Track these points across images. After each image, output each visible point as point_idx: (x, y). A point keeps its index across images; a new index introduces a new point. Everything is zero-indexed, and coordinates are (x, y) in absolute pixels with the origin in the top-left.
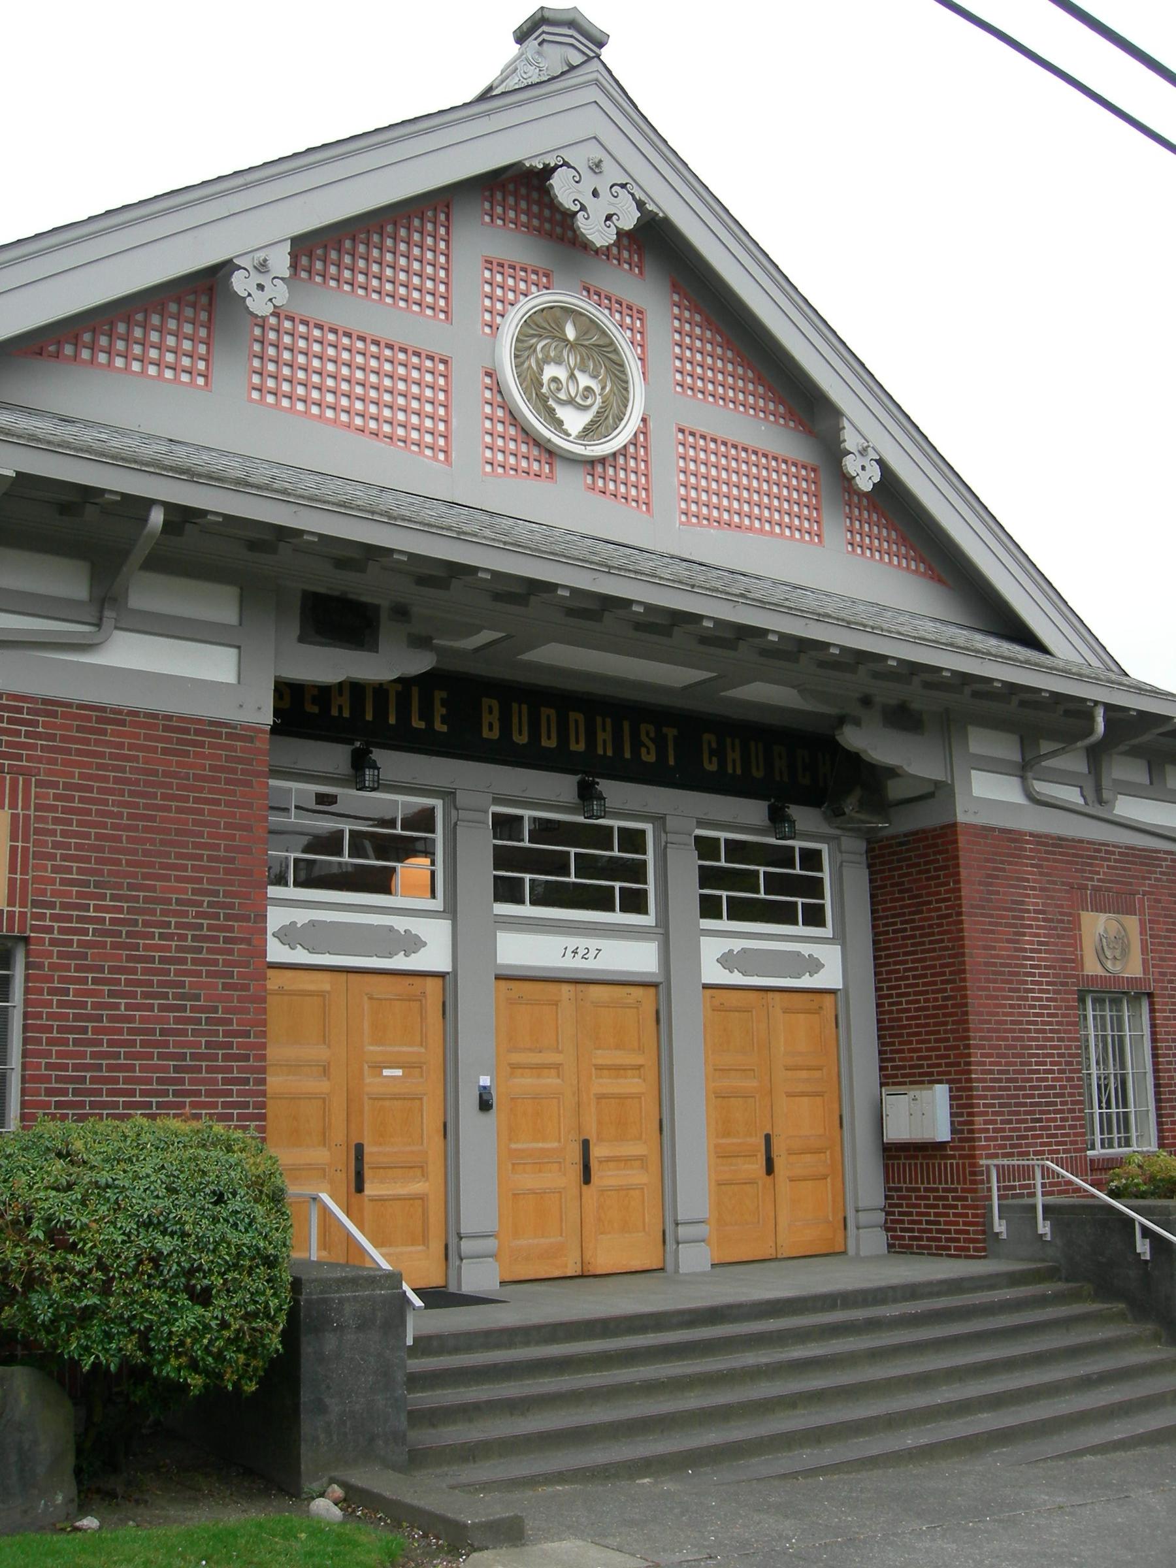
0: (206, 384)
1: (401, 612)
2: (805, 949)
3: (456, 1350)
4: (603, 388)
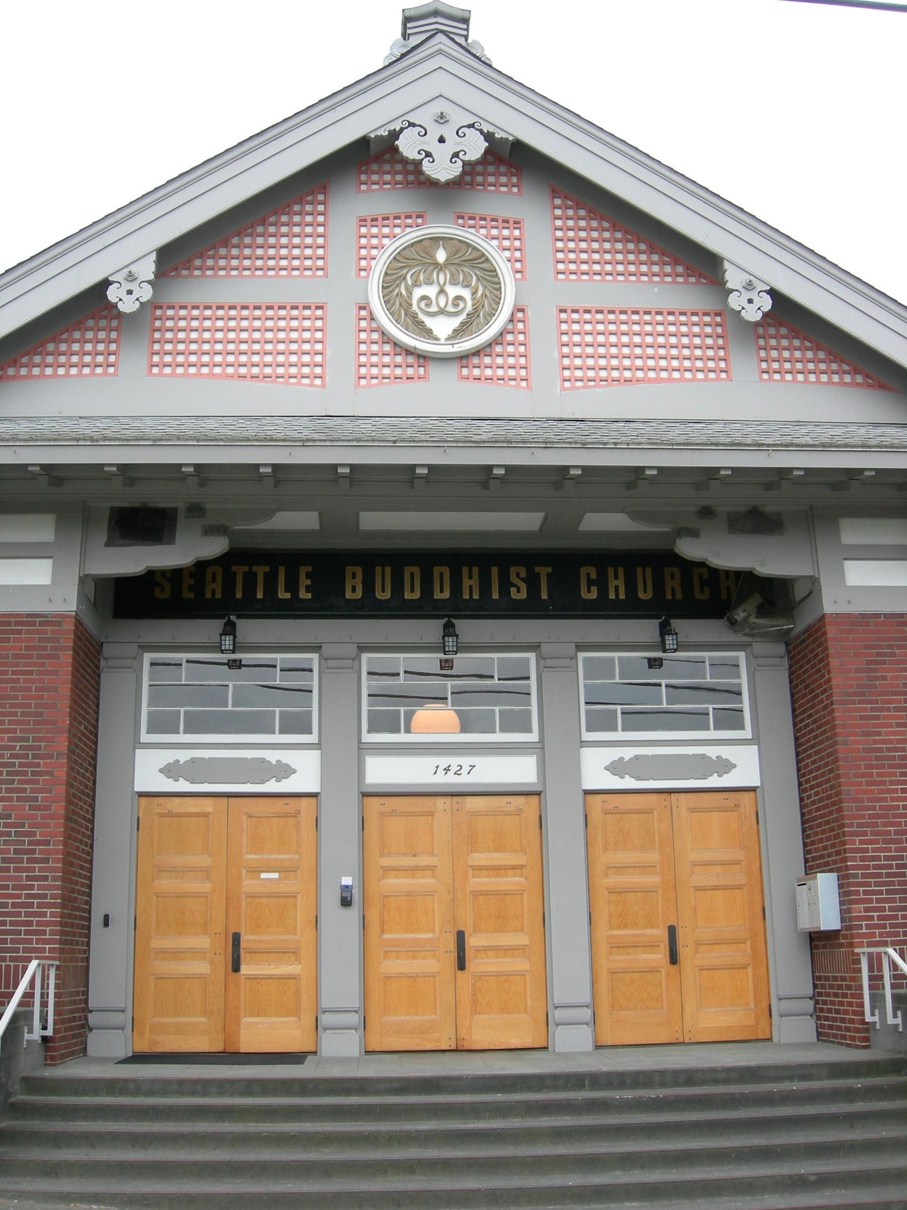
0: (728, 377)
1: (196, 510)
2: (712, 752)
3: (151, 1093)
4: (474, 293)
